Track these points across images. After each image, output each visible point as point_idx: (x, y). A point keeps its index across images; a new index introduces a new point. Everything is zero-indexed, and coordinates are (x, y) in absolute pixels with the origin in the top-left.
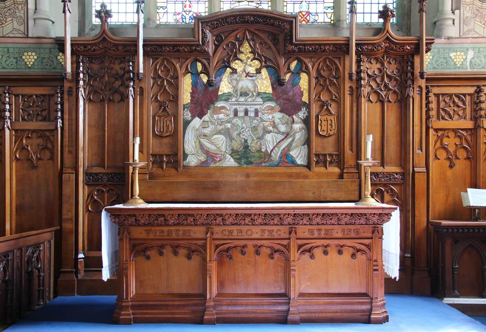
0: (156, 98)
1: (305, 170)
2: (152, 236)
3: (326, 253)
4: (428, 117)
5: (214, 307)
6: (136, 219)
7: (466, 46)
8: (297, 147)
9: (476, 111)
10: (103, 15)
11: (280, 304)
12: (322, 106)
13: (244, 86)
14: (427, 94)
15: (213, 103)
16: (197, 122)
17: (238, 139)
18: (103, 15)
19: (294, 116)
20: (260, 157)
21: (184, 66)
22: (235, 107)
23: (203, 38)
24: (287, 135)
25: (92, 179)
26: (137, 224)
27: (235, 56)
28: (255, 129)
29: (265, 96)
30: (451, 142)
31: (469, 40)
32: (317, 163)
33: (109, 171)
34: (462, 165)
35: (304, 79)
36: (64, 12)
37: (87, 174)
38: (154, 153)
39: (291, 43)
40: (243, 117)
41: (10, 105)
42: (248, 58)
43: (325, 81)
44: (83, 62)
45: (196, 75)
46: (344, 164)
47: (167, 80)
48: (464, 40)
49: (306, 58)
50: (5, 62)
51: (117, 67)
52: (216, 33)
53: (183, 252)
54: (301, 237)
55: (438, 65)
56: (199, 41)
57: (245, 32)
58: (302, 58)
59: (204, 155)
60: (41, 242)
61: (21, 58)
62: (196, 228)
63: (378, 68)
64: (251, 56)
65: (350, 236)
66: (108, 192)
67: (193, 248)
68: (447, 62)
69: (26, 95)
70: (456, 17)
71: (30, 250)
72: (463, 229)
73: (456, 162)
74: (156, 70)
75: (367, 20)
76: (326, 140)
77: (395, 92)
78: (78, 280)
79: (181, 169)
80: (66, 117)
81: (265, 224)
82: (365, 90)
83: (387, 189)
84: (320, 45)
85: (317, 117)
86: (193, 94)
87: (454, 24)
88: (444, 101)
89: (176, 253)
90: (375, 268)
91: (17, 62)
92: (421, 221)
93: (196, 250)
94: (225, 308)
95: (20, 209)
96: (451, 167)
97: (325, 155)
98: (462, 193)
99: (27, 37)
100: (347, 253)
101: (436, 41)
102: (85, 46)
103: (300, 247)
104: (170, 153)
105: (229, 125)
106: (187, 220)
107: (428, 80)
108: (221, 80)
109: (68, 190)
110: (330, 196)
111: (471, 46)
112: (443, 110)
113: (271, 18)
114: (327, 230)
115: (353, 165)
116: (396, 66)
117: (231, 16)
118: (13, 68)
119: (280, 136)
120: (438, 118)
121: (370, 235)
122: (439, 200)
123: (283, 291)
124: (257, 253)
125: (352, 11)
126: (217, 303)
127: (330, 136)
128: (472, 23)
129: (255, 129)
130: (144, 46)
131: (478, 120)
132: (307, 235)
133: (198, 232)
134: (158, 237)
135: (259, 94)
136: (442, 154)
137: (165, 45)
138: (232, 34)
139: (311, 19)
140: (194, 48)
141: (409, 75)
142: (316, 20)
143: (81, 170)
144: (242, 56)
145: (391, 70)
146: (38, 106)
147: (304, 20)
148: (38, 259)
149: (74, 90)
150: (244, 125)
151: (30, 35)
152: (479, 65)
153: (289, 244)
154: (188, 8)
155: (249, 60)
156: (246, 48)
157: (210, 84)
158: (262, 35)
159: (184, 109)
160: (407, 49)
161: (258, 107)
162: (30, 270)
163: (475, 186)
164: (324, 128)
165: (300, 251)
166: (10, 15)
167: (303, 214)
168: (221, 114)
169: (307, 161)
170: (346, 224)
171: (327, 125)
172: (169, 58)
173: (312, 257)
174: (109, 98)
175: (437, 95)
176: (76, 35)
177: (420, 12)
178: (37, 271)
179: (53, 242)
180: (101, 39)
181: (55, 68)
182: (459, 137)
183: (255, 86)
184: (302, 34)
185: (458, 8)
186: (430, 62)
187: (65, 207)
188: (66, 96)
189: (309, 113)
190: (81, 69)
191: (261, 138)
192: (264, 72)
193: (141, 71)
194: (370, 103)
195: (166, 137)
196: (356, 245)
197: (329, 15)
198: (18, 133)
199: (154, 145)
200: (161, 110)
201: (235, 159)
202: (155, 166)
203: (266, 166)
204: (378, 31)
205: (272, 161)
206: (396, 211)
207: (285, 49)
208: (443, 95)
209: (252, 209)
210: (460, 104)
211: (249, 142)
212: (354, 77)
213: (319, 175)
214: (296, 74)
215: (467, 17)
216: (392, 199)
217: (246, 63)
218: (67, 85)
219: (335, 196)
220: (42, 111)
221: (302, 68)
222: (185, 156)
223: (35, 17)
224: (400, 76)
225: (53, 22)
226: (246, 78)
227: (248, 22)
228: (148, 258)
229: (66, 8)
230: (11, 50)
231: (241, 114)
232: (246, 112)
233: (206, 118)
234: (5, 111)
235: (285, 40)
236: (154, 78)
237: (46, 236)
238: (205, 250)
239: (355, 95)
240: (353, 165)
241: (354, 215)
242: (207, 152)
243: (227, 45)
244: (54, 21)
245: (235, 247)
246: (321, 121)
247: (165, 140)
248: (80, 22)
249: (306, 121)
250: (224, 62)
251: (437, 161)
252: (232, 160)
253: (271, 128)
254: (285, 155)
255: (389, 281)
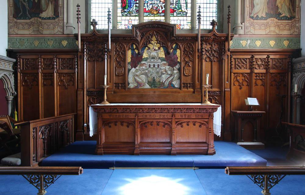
0: (117, 60)
1: (179, 90)
2: (112, 118)
3: (188, 125)
4: (231, 68)
5: (139, 147)
6: (104, 110)
7: (247, 38)
8: (175, 80)
9: (251, 65)
11: (168, 146)
12: (186, 63)
13: (153, 55)
14: (231, 58)
15: (140, 61)
16: (133, 70)
17: (151, 77)
18: (94, 24)
19: (174, 68)
20: (160, 84)
21: (128, 46)
22: (149, 63)
23: (136, 34)
24: (171, 75)
25: (90, 93)
26: (105, 112)
27: (150, 42)
28: (158, 73)
29: (162, 59)
30: (240, 78)
31: (248, 36)
32: (184, 87)
33: (97, 90)
34: (245, 88)
35: (178, 52)
36: (78, 23)
37: (87, 91)
38: (116, 82)
39: (173, 36)
40: (153, 67)
41: (57, 63)
42: (155, 43)
43: (187, 53)
44: (86, 44)
45: (133, 50)
46: (195, 88)
47: (189, 52)
48: (246, 36)
49: (179, 43)
50: (27, 45)
51: (100, 46)
52: (141, 32)
53: (125, 124)
54: (177, 118)
55: (235, 46)
56: (134, 35)
57: (154, 32)
58: (178, 43)
59: (137, 84)
60: (68, 119)
61: (269, 43)
62: (131, 114)
63: (210, 47)
64: (156, 42)
65: (199, 118)
66: (96, 99)
67: (130, 123)
68: (239, 45)
69: (63, 58)
70: (243, 26)
71: (62, 123)
72: (242, 114)
73: (243, 87)
74: (116, 48)
75: (205, 28)
76: (188, 77)
77: (217, 57)
78: (84, 134)
79: (127, 89)
80: (79, 67)
81: (161, 112)
82: (204, 57)
83: (213, 98)
84: (185, 37)
85: (184, 68)
86: (132, 58)
87: (242, 28)
88: (238, 61)
89: (122, 125)
90: (210, 131)
91: (31, 45)
92: (228, 111)
93: (131, 123)
94: (144, 148)
95: (61, 105)
96: (240, 89)
97: (187, 84)
98: (245, 100)
99: (64, 34)
100: (197, 125)
101: (235, 36)
102: (86, 37)
103: (176, 122)
104: (122, 83)
105: (147, 71)
106: (127, 111)
107: (231, 52)
108: (143, 52)
109: (80, 98)
110: (189, 101)
111: (249, 38)
112: (237, 65)
113: (165, 25)
114: (189, 115)
115: (199, 87)
116: (217, 46)
117: (148, 24)
118: (29, 47)
119: (168, 75)
120: (235, 69)
121: (208, 117)
122: (235, 102)
123: (169, 141)
124: (158, 125)
125: (199, 22)
126: (140, 146)
127: (189, 76)
128: (250, 28)
129: (158, 73)
130: (111, 37)
131: (252, 69)
132: (180, 117)
133: (132, 116)
134: (114, 118)
135: (159, 58)
136: (237, 84)
137: (120, 37)
138: (148, 33)
139: (182, 27)
140: (132, 38)
141: (223, 50)
143: (85, 90)
144: (153, 42)
145: (215, 48)
146: (68, 63)
148: (66, 126)
149: (82, 56)
150: (153, 71)
151: (65, 33)
152: (252, 46)
153: (172, 121)
154: (130, 23)
155: (155, 44)
156: (154, 38)
157: (139, 53)
158: (160, 33)
159: (128, 65)
160: (222, 39)
161: (159, 63)
162: (62, 131)
163: (251, 97)
164: (187, 72)
165: (176, 124)
166: (57, 25)
167: (178, 108)
168: (144, 66)
169: (179, 86)
170: (197, 113)
171: (188, 71)
172: (121, 42)
173: (182, 126)
174: (97, 60)
175: (235, 59)
176: (84, 32)
177: (228, 23)
178: (66, 131)
179: (73, 119)
180: (93, 34)
181: (75, 47)
182: (244, 76)
183: (158, 55)
184: (177, 32)
185: (244, 22)
186: (232, 44)
187: (79, 105)
188: (79, 59)
189: (181, 66)
190: (85, 47)
191: (160, 76)
192: (162, 49)
193: (110, 48)
194: (206, 62)
195: (121, 76)
196: (201, 121)
197: (189, 26)
198: (60, 74)
199: (115, 78)
200: (118, 65)
201: (149, 85)
202: (116, 88)
203: (162, 88)
204: (210, 31)
205: (165, 86)
206: (219, 107)
207: (170, 39)
208: (237, 59)
209: (158, 106)
210: (245, 63)
211: (155, 78)
212: (200, 51)
213: (184, 92)
214: (175, 50)
215: (247, 26)
216: (215, 102)
217: (154, 45)
218: (79, 54)
219: (191, 100)
220: (69, 65)
221: (178, 47)
222: (129, 84)
223: (66, 26)
224: (219, 51)
225: (74, 28)
226: (154, 52)
227: (155, 27)
228: (110, 127)
229: (79, 21)
230: (57, 40)
231: (152, 66)
232: (154, 66)
233: (137, 68)
234: (54, 65)
235: (170, 35)
236: (115, 51)
237: (70, 118)
238: (135, 124)
239: (200, 59)
240: (199, 87)
241: (200, 109)
242: (138, 82)
243: (146, 37)
244: (75, 27)
245: (148, 122)
246: (186, 69)
247: (120, 77)
248: (86, 28)
249: (179, 70)
250: (145, 44)
251: (235, 86)
252: (148, 86)
253: (164, 72)
254: (170, 83)
255: (215, 135)
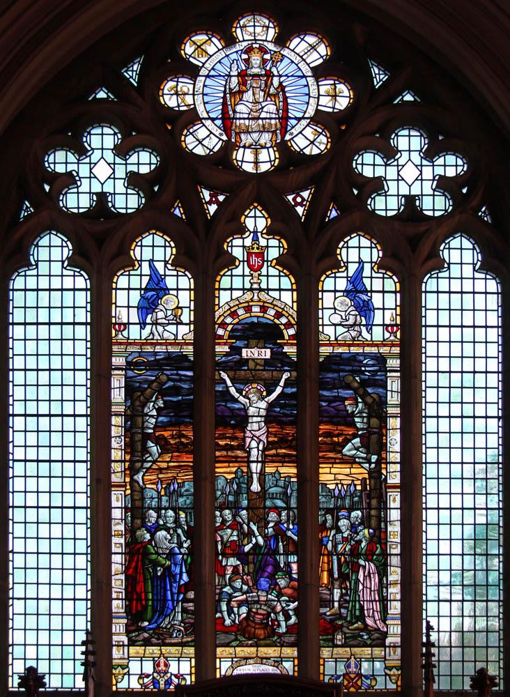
10: (31, 683)
142: (373, 687)
147: (352, 686)
